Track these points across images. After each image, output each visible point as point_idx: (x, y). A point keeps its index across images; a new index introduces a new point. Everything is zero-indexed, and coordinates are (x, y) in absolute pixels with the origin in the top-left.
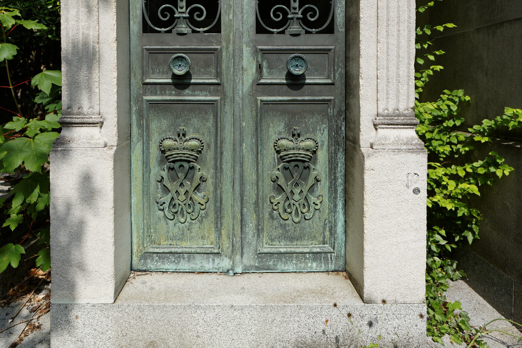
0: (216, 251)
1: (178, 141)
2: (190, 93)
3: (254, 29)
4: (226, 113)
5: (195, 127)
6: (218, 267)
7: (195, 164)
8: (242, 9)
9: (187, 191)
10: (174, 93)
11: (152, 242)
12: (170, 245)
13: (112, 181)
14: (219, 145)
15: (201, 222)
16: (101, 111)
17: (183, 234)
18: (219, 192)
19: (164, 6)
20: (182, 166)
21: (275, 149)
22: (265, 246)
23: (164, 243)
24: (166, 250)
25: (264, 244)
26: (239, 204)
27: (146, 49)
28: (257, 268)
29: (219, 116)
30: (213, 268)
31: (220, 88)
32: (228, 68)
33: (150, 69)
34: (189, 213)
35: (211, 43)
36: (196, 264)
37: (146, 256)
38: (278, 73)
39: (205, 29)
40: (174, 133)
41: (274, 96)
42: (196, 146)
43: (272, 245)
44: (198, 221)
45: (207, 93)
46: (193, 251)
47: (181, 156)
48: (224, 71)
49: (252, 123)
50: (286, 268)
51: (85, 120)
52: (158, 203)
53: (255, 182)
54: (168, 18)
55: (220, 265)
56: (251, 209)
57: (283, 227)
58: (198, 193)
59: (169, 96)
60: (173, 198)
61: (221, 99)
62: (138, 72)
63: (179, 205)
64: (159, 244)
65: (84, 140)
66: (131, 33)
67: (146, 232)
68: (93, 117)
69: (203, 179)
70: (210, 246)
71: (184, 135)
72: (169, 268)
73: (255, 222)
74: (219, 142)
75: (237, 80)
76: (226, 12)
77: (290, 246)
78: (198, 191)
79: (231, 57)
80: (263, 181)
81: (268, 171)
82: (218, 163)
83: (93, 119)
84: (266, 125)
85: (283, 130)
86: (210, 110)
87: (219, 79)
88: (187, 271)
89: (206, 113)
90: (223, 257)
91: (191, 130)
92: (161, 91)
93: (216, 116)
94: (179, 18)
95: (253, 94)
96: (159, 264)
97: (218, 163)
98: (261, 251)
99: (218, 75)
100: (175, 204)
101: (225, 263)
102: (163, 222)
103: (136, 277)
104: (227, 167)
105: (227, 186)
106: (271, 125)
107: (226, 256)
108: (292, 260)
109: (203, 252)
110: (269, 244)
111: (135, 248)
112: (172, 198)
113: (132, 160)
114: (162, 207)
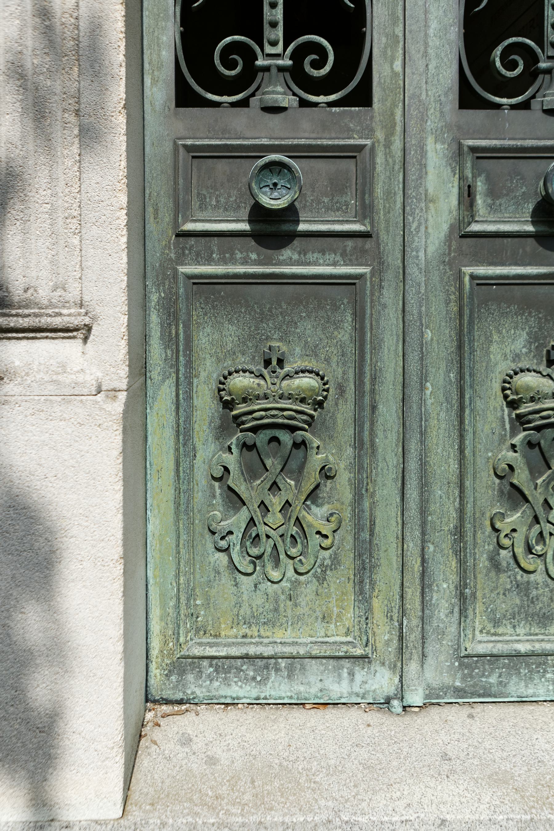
0: (359, 652)
1: (267, 377)
2: (296, 257)
3: (454, 96)
4: (385, 306)
5: (306, 342)
6: (362, 691)
7: (308, 435)
8: (426, 45)
9: (287, 501)
10: (254, 256)
11: (198, 630)
12: (245, 636)
13: (119, 486)
14: (367, 387)
15: (321, 579)
16: (86, 298)
17: (276, 610)
18: (366, 504)
19: (228, 39)
20: (275, 439)
21: (506, 397)
22: (479, 637)
23: (228, 632)
24: (234, 651)
25: (477, 633)
26: (418, 533)
27: (185, 146)
28: (460, 692)
29: (368, 316)
30: (351, 694)
31: (369, 244)
32: (389, 194)
33: (195, 198)
34: (292, 558)
35: (348, 132)
36: (309, 684)
37: (183, 665)
38: (512, 208)
39: (333, 97)
40: (254, 357)
41: (503, 264)
42: (312, 389)
43: (495, 634)
44: (315, 576)
45: (338, 258)
46: (302, 651)
47: (273, 416)
48: (380, 204)
49: (448, 333)
50: (530, 691)
51: (44, 321)
52: (213, 533)
53: (454, 479)
54: (239, 69)
55: (367, 686)
56: (444, 546)
57: (524, 589)
58: (313, 507)
59: (242, 264)
60: (252, 519)
61: (373, 273)
62: (166, 205)
63: (268, 537)
64: (216, 636)
65: (41, 375)
66: (147, 107)
67: (183, 607)
68: (65, 311)
69: (327, 474)
70: (344, 639)
71: (280, 362)
72: (241, 694)
73: (454, 578)
74: (367, 380)
75: (414, 226)
76: (385, 53)
77: (540, 637)
78: (313, 503)
79: (397, 167)
80: (475, 478)
81: (487, 450)
82: (366, 433)
83: (66, 319)
84: (483, 338)
85: (524, 350)
86: (345, 301)
87: (367, 221)
88: (286, 701)
89: (335, 308)
90: (376, 666)
91: (298, 350)
92: (222, 252)
93: (359, 316)
94: (267, 69)
95: (451, 261)
96: (216, 684)
97: (366, 433)
98: (469, 651)
99: (366, 211)
100: (257, 536)
101: (382, 681)
102: (226, 579)
103: (162, 722)
104: (387, 442)
105: (386, 489)
106: (495, 337)
107: (383, 664)
108: (545, 671)
109: (328, 654)
110: (488, 633)
111: (156, 644)
112: (252, 522)
113: (149, 426)
114: (223, 544)
